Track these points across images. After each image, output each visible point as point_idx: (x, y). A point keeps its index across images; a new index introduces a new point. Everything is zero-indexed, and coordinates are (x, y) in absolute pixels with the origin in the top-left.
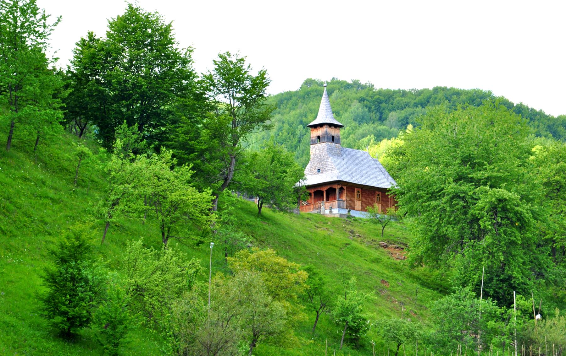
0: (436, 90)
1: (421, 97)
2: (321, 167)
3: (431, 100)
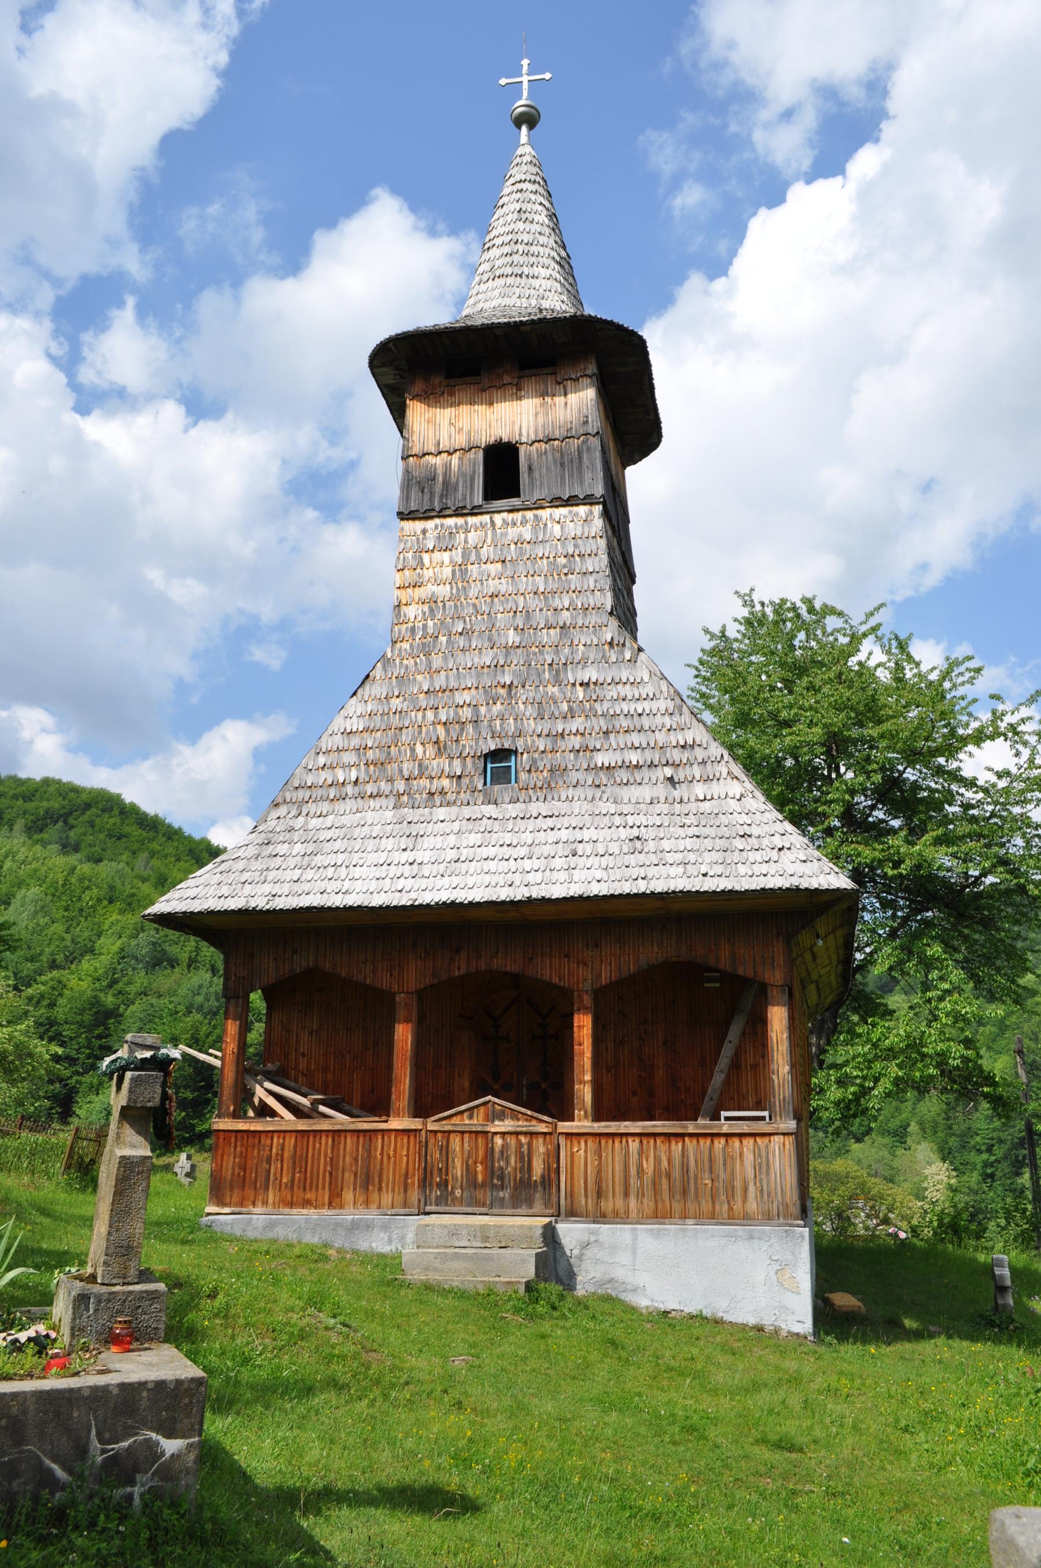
0: (47, 782)
1: (24, 788)
2: (524, 725)
3: (38, 795)
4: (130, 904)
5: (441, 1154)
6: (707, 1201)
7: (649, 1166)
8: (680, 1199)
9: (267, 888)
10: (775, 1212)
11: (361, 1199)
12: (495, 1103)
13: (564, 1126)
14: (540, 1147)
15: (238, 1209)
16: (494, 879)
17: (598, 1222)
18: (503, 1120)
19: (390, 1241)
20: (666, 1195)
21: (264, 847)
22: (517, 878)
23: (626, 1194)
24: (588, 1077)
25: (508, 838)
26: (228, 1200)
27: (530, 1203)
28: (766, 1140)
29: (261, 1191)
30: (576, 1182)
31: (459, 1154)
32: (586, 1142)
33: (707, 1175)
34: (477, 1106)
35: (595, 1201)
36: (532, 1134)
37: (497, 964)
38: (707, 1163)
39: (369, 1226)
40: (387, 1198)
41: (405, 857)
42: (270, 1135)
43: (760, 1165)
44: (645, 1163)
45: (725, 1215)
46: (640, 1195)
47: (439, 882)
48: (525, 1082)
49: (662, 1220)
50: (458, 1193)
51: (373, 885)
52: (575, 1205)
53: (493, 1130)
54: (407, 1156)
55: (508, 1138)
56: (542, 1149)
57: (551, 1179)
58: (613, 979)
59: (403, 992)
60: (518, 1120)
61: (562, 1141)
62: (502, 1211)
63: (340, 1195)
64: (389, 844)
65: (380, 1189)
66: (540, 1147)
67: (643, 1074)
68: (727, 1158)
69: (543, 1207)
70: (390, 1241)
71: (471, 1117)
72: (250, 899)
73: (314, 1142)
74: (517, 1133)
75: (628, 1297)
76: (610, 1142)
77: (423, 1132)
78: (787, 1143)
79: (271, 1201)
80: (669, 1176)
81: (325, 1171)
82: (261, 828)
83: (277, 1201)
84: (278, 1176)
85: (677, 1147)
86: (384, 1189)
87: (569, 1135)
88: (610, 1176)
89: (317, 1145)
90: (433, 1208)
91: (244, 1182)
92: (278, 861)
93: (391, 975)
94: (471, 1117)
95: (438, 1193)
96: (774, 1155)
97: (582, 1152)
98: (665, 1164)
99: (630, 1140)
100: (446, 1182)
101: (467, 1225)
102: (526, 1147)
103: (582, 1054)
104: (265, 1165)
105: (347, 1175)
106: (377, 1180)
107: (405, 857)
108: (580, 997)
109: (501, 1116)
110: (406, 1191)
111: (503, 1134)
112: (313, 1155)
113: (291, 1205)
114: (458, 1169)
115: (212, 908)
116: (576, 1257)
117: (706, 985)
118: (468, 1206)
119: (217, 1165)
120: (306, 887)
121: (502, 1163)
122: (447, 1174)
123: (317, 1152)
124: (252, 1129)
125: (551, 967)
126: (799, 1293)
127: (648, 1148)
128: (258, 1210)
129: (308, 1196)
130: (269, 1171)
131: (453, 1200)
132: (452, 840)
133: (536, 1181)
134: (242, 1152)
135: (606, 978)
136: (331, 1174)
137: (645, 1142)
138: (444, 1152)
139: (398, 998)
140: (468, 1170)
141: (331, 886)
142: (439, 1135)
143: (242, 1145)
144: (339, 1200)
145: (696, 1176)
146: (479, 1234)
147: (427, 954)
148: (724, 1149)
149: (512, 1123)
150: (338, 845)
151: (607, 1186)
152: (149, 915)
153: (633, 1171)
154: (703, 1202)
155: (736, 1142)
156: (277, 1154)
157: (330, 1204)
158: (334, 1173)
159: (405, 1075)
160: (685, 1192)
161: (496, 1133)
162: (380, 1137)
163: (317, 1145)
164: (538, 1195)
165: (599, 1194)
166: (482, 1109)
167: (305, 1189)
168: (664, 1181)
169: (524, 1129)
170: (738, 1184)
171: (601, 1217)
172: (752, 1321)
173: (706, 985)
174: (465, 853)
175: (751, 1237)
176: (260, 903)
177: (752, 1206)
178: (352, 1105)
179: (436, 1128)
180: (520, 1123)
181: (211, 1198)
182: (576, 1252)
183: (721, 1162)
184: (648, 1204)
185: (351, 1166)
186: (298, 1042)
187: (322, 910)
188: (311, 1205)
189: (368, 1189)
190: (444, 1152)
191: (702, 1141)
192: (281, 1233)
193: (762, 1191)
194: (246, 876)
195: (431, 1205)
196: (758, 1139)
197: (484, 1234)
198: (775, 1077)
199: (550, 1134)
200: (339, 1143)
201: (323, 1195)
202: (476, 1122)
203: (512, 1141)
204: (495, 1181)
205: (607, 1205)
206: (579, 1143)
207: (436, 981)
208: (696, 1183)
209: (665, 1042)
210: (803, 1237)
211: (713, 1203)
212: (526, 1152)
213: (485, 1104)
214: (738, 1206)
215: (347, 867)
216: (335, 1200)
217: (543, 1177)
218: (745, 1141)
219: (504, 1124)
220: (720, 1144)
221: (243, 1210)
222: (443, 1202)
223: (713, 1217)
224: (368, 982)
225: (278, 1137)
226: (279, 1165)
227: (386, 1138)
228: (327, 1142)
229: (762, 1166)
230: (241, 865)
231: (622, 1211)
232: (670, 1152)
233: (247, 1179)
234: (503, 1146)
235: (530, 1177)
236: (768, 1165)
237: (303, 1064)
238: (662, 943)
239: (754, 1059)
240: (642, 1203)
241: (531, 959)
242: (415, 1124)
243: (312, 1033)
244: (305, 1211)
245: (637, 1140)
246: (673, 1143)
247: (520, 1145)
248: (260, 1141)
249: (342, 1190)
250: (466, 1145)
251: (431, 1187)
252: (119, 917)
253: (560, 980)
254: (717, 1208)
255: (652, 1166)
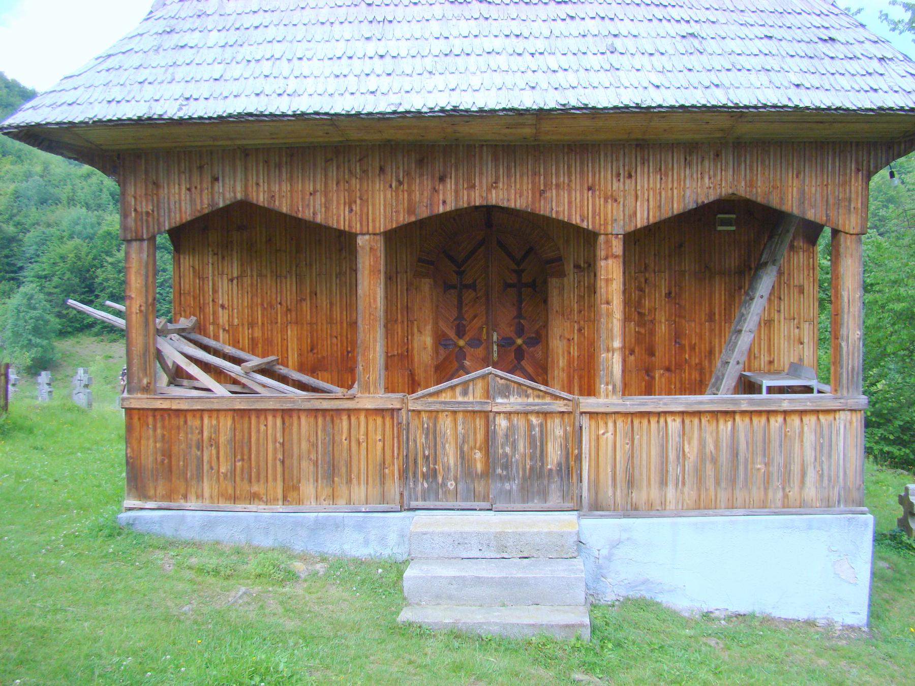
4: (19, 157)
5: (427, 438)
6: (759, 488)
7: (691, 450)
8: (727, 486)
9: (177, 90)
10: (836, 498)
11: (327, 491)
12: (497, 376)
13: (588, 403)
14: (557, 429)
15: (165, 504)
16: (509, 79)
17: (628, 516)
18: (508, 397)
19: (366, 543)
20: (710, 483)
21: (166, 36)
22: (542, 79)
23: (663, 483)
24: (617, 344)
25: (516, 27)
26: (152, 492)
27: (544, 494)
28: (830, 417)
29: (194, 482)
30: (601, 470)
31: (451, 440)
32: (615, 423)
33: (759, 459)
34: (473, 380)
35: (625, 492)
36: (546, 414)
37: (497, 197)
38: (760, 445)
39: (338, 526)
40: (359, 492)
41: (371, 48)
42: (198, 415)
43: (822, 445)
44: (686, 446)
45: (779, 503)
46: (681, 483)
47: (430, 82)
48: (495, 338)
49: (706, 511)
50: (451, 485)
51: (332, 85)
52: (600, 496)
53: (495, 409)
54: (383, 440)
55: (515, 420)
56: (559, 432)
57: (569, 469)
58: (652, 221)
59: (368, 233)
60: (528, 396)
61: (585, 421)
62: (510, 506)
63: (296, 488)
64: (347, 31)
65: (349, 481)
66: (557, 429)
67: (643, 331)
68: (785, 437)
69: (560, 500)
70: (366, 543)
71: (465, 393)
72: (155, 103)
73: (258, 423)
74: (526, 413)
75: (664, 599)
76: (645, 422)
77: (403, 412)
78: (854, 420)
79: (207, 494)
80: (714, 461)
81: (275, 459)
82: (158, 14)
83: (215, 492)
84: (214, 464)
85: (725, 427)
86: (355, 481)
87: (592, 415)
88: (644, 463)
89: (262, 428)
90: (420, 504)
91: (171, 470)
92: (188, 54)
93: (351, 210)
94: (465, 393)
95: (426, 485)
96: (838, 434)
97: (609, 435)
98: (710, 446)
99: (669, 419)
100: (435, 473)
101: (478, 533)
102: (537, 429)
103: (609, 314)
104: (195, 451)
105: (304, 464)
106: (344, 470)
107: (371, 48)
108: (608, 242)
109: (505, 392)
110: (383, 483)
111: (508, 414)
112: (258, 439)
113: (235, 499)
114: (450, 456)
115: (100, 117)
116: (605, 558)
117: (720, 228)
118: (466, 499)
119: (133, 450)
120: (235, 87)
121: (508, 450)
122: (435, 463)
123: (262, 436)
124: (174, 407)
125: (570, 203)
126: (856, 584)
127: (692, 428)
128: (193, 503)
129: (255, 488)
130: (200, 460)
131: (445, 493)
132: (435, 28)
133: (551, 470)
134: (163, 436)
135: (642, 218)
136: (283, 462)
137: (687, 421)
138: (431, 436)
139: (360, 241)
140: (463, 458)
141: (270, 86)
142: (424, 416)
143: (163, 427)
144: (295, 494)
145: (746, 460)
146: (493, 543)
147: (400, 183)
148: (780, 428)
149: (519, 400)
150: (271, 33)
151: (641, 474)
152: (10, 126)
153: (672, 456)
154: (754, 490)
155: (795, 420)
156: (210, 439)
157: (285, 498)
158: (287, 462)
159: (375, 340)
160: (733, 481)
161: (499, 413)
162: (345, 418)
163: (262, 428)
164: (553, 486)
165: (631, 483)
166: (480, 384)
167: (250, 481)
168: (709, 467)
169: (536, 408)
170: (796, 469)
171: (632, 510)
172: (802, 615)
173: (720, 228)
174: (458, 45)
175: (810, 527)
176: (170, 110)
177: (811, 492)
178: (287, 366)
179: (419, 408)
180: (530, 400)
181: (130, 490)
182: (604, 552)
183: (777, 443)
184: (690, 493)
185: (309, 452)
186: (215, 291)
187: (258, 119)
188: (260, 499)
189: (333, 482)
190: (431, 436)
191: (755, 420)
192: (222, 533)
193: (822, 476)
194: (143, 74)
195: (417, 500)
196: (821, 417)
197: (502, 548)
198: (844, 344)
199: (569, 413)
200: (292, 425)
201: (275, 488)
202: (474, 397)
203: (520, 422)
204: (499, 471)
205: (640, 496)
206: (606, 423)
207: (413, 219)
208: (746, 468)
209: (668, 295)
210: (866, 525)
211: (766, 489)
212: (538, 435)
213: (483, 377)
214: (793, 494)
215: (289, 60)
216: (290, 493)
217: (559, 464)
218: (806, 419)
219: (510, 402)
220: (776, 422)
221: (173, 504)
222: (432, 496)
223: (763, 506)
224: (319, 219)
225: (210, 417)
226: (214, 452)
227: (353, 419)
228: (275, 424)
229: (824, 447)
230: (135, 60)
231: (658, 502)
232: (717, 432)
233: (174, 468)
234: (508, 428)
235: (542, 466)
236: (830, 445)
237: (223, 317)
238: (715, 176)
239: (769, 314)
240: (682, 492)
241: (542, 193)
242: (392, 401)
243: (232, 280)
244: (253, 507)
245: (678, 420)
246: (721, 421)
247: (531, 427)
248: (186, 422)
249: (300, 482)
250: (460, 428)
251: (416, 479)
252: (12, 167)
253: (582, 221)
254: (770, 495)
255: (695, 450)
